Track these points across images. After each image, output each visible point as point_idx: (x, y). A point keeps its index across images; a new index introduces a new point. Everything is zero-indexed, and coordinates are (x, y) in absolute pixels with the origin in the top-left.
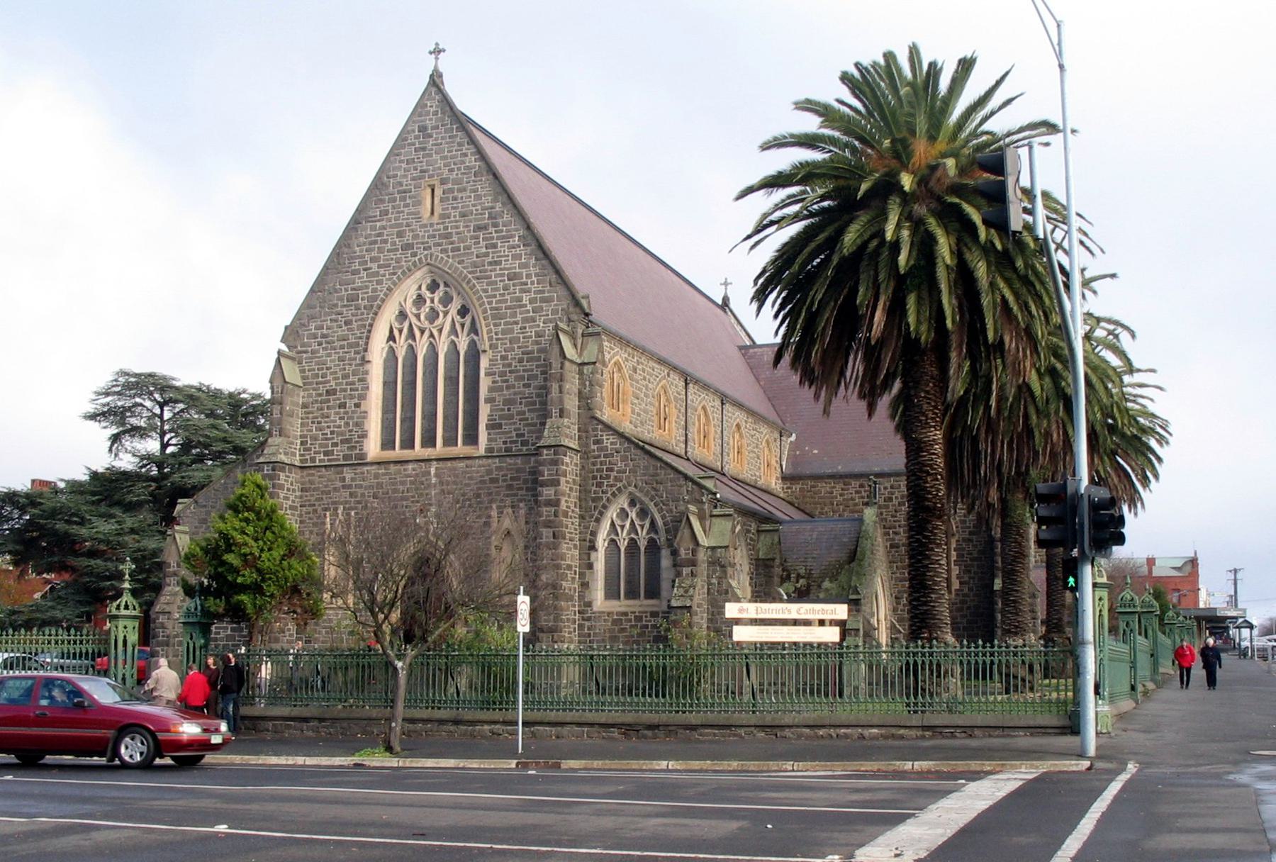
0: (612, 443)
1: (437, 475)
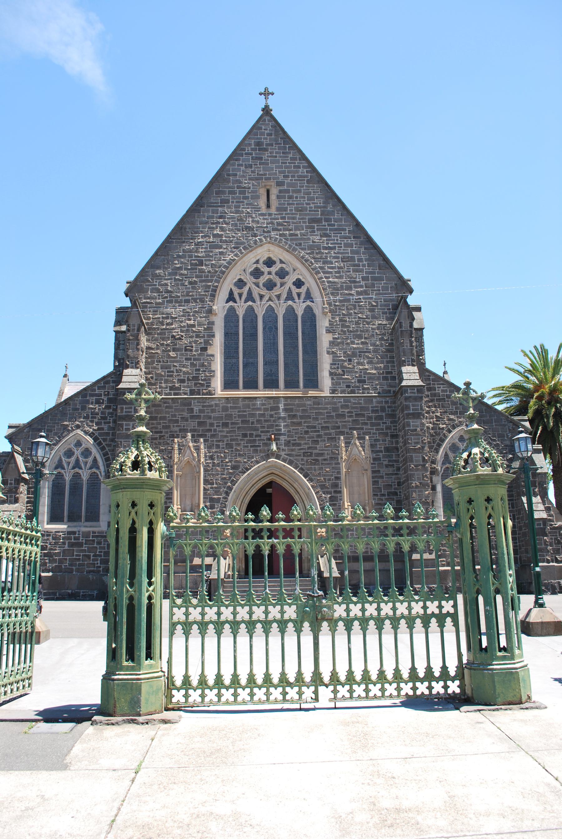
0: (443, 391)
1: (285, 410)
